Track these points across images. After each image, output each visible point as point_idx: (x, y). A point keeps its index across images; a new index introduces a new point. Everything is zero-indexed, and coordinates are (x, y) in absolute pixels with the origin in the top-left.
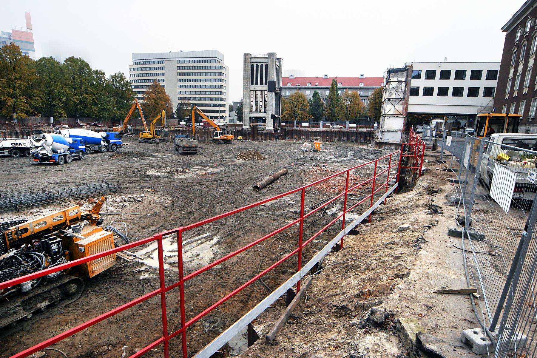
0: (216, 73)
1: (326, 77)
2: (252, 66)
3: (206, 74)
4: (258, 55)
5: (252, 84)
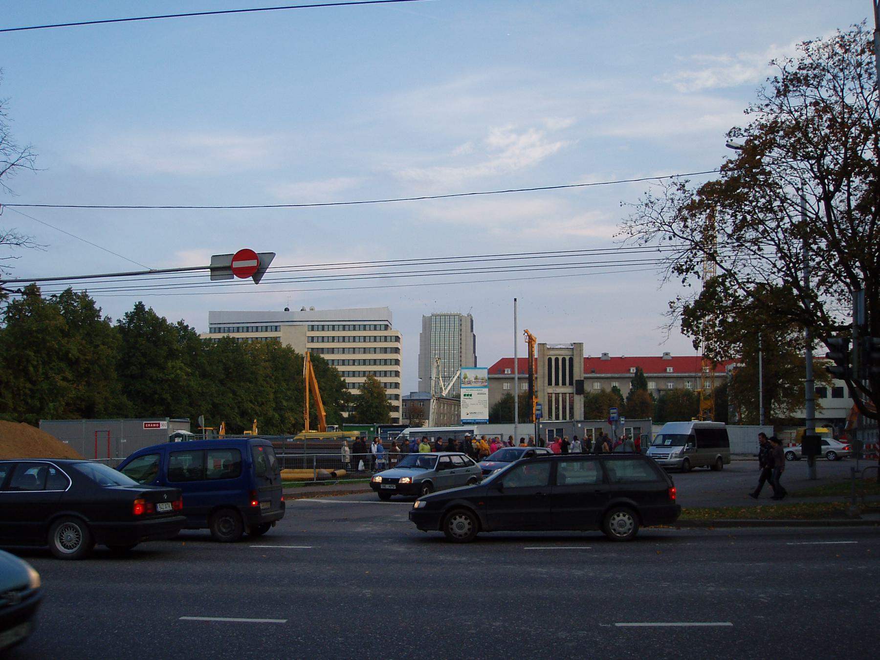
0: (386, 348)
1: (605, 358)
2: (550, 360)
3: (365, 350)
4: (557, 345)
5: (550, 384)
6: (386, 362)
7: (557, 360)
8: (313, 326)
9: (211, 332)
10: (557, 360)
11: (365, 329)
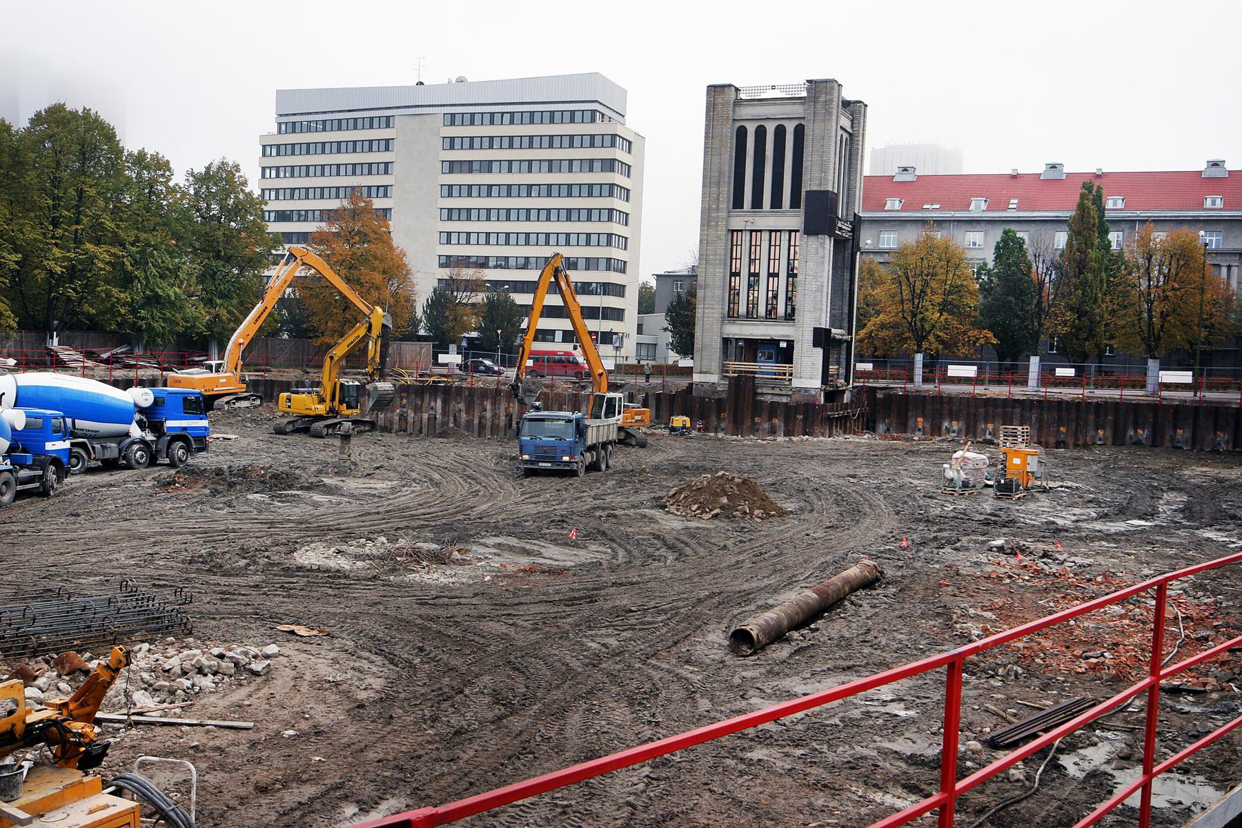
0: (591, 161)
1: (1053, 175)
2: (741, 133)
4: (764, 89)
5: (738, 203)
6: (590, 190)
7: (761, 133)
8: (453, 115)
9: (280, 132)
10: (761, 133)
11: (552, 121)
